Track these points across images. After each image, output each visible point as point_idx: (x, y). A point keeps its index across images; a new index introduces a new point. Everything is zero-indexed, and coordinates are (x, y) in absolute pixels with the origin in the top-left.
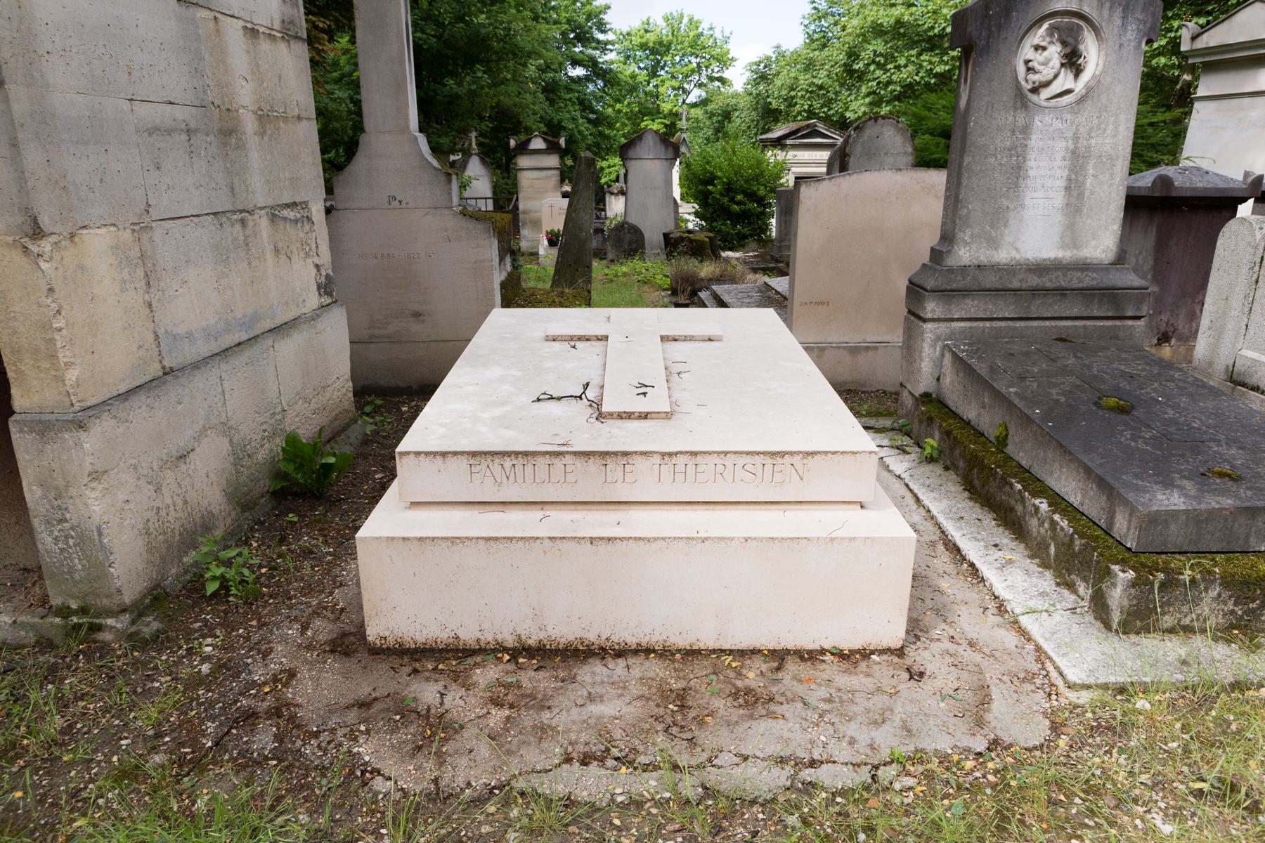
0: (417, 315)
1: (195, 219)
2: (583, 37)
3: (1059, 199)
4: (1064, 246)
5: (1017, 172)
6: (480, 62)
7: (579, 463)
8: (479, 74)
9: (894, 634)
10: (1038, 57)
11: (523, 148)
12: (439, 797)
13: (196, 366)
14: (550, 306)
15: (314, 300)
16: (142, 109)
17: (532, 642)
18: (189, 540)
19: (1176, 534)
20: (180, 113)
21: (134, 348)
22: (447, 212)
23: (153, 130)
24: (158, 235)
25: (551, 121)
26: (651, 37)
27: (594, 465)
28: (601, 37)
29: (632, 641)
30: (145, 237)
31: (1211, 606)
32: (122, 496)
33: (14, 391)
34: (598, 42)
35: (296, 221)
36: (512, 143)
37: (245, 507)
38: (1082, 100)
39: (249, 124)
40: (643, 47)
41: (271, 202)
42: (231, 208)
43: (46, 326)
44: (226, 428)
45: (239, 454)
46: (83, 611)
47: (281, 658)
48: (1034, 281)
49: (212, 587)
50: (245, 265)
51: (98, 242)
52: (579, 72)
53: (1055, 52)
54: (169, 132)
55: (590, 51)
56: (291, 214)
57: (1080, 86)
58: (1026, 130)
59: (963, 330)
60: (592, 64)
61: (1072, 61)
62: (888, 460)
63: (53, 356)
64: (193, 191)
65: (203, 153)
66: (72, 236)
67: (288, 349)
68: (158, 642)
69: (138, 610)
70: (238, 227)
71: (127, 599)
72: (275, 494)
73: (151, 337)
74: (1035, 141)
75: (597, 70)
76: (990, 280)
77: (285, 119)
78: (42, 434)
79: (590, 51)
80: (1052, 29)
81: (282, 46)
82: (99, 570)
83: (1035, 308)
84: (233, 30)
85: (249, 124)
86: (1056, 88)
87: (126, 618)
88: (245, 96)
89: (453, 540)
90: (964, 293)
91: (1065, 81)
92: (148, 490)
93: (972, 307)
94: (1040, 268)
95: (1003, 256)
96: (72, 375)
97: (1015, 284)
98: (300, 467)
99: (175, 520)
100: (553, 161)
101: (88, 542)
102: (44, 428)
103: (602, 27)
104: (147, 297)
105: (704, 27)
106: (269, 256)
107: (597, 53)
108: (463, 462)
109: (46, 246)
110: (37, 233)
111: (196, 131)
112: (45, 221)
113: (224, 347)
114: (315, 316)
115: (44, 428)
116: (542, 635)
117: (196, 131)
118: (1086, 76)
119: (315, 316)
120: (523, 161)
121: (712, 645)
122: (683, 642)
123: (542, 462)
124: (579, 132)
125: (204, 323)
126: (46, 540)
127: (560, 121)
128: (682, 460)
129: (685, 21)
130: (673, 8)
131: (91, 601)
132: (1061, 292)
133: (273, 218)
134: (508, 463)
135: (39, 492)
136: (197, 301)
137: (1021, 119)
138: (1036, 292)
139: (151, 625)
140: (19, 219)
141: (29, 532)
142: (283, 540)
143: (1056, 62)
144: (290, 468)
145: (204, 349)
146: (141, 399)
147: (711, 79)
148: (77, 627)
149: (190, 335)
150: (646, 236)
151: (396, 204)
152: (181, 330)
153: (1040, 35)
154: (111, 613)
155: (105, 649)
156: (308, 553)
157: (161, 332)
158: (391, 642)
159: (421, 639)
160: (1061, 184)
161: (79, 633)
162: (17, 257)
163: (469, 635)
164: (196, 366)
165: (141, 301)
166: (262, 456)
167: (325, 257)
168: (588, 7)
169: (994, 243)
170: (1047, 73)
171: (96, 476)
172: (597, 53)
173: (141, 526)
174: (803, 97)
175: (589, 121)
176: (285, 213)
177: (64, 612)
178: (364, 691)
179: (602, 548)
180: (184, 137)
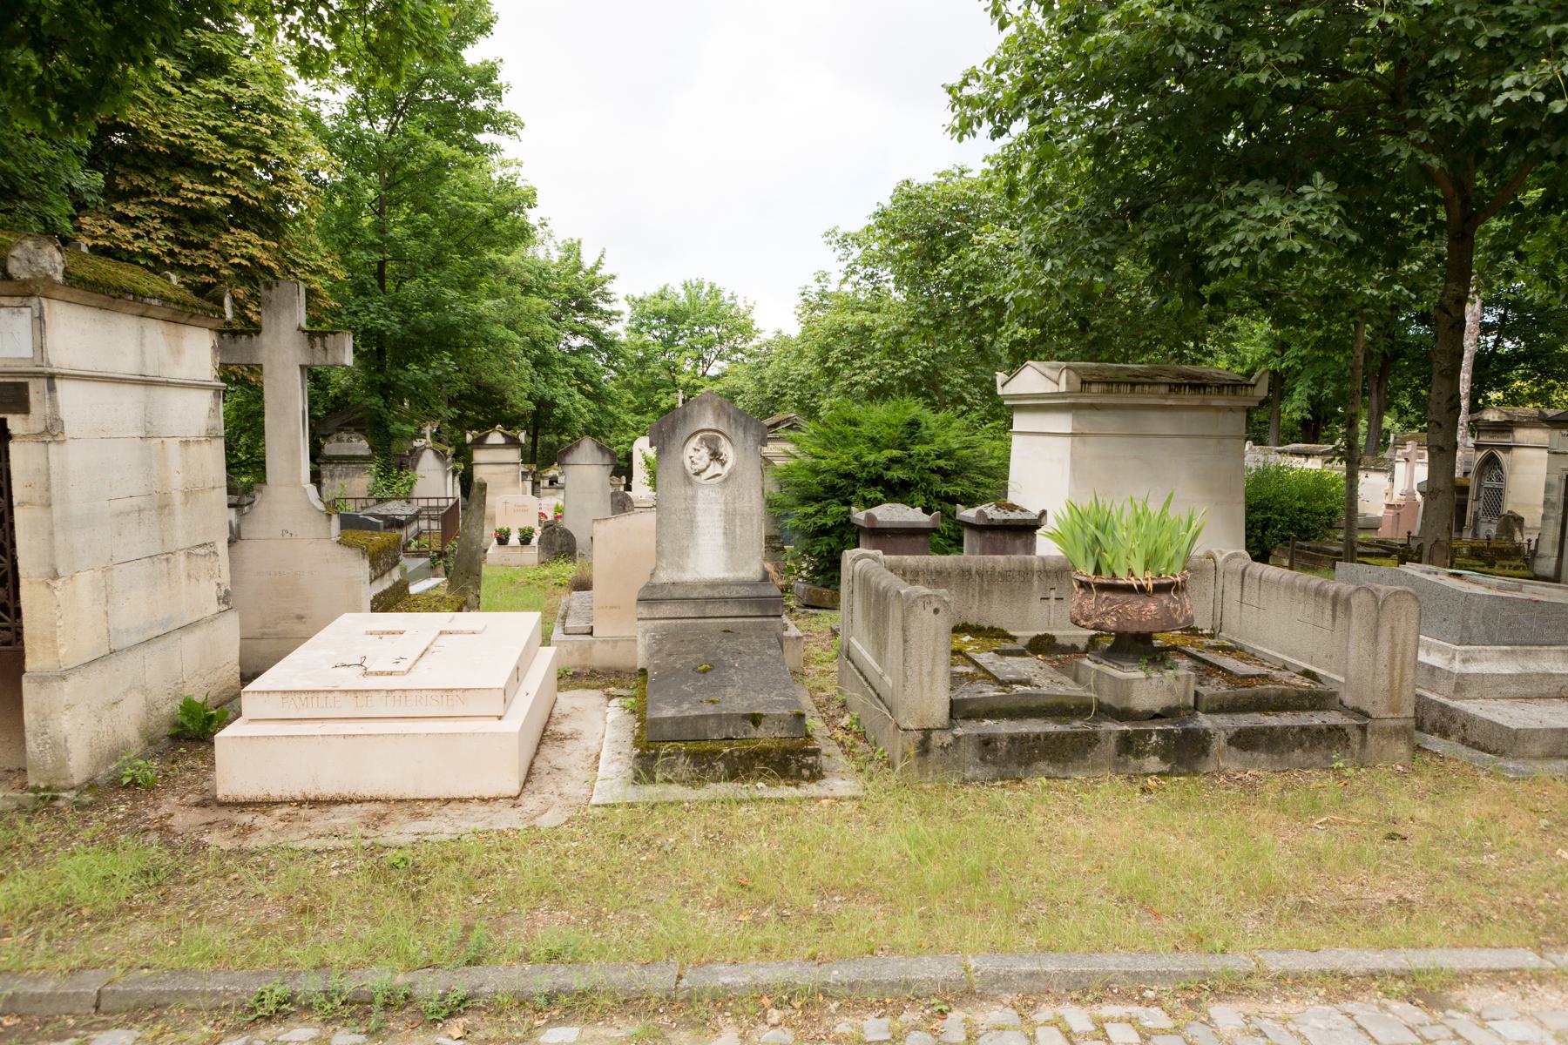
0: (300, 617)
2: (585, 307)
3: (720, 540)
4: (728, 570)
5: (691, 523)
6: (448, 347)
7: (343, 695)
8: (446, 361)
9: (513, 787)
10: (696, 455)
11: (480, 443)
13: (129, 649)
14: (426, 610)
15: (214, 607)
16: (115, 504)
17: (311, 797)
18: (114, 755)
19: (667, 730)
20: (135, 502)
23: (120, 514)
25: (542, 398)
26: (666, 306)
27: (350, 697)
28: (606, 307)
29: (368, 795)
31: (683, 767)
33: (27, 660)
34: (602, 312)
36: (469, 438)
37: (151, 743)
38: (726, 480)
39: (178, 498)
40: (658, 315)
43: (53, 625)
44: (144, 690)
45: (151, 707)
46: (48, 789)
47: (165, 809)
48: (708, 593)
49: (126, 780)
51: (84, 579)
52: (577, 343)
53: (705, 452)
54: (128, 514)
55: (593, 322)
56: (201, 551)
57: (724, 471)
58: (693, 498)
59: (662, 626)
60: (595, 335)
61: (716, 456)
63: (54, 641)
67: (190, 641)
68: (90, 806)
69: (80, 789)
71: (76, 781)
72: (171, 737)
74: (700, 505)
75: (603, 343)
76: (678, 593)
78: (41, 683)
79: (593, 322)
80: (702, 439)
81: (206, 445)
82: (62, 763)
83: (709, 611)
84: (173, 446)
85: (178, 498)
86: (709, 473)
87: (74, 793)
88: (177, 482)
89: (268, 737)
90: (661, 601)
91: (716, 468)
92: (94, 720)
93: (665, 610)
94: (713, 585)
95: (688, 577)
96: (62, 651)
97: (695, 595)
98: (192, 719)
99: (107, 742)
100: (513, 455)
101: (58, 746)
102: (42, 680)
103: (605, 297)
105: (726, 295)
107: (599, 323)
108: (279, 696)
109: (59, 583)
110: (56, 576)
112: (60, 571)
114: (213, 619)
115: (42, 680)
116: (317, 792)
118: (728, 466)
119: (213, 619)
120: (479, 456)
121: (413, 796)
122: (397, 795)
123: (322, 695)
124: (575, 409)
126: (32, 745)
127: (553, 398)
128: (397, 694)
129: (706, 289)
130: (692, 276)
131: (53, 782)
132: (725, 600)
133: (189, 555)
134: (303, 696)
135: (32, 717)
136: (136, 608)
137: (689, 491)
138: (708, 600)
139: (88, 798)
140: (47, 569)
141: (23, 741)
142: (174, 762)
143: (707, 458)
144: (185, 719)
145: (136, 639)
146: (96, 666)
147: (735, 350)
148: (43, 798)
149: (127, 631)
150: (578, 541)
153: (694, 442)
154: (65, 790)
155: (59, 810)
156: (191, 769)
158: (231, 799)
159: (248, 796)
160: (721, 531)
161: (46, 801)
162: (43, 588)
163: (276, 794)
164: (129, 649)
166: (166, 710)
167: (226, 578)
168: (591, 276)
169: (681, 568)
170: (701, 465)
171: (69, 707)
172: (599, 323)
174: (792, 388)
175: (588, 396)
177: (36, 790)
178: (211, 819)
179: (350, 740)
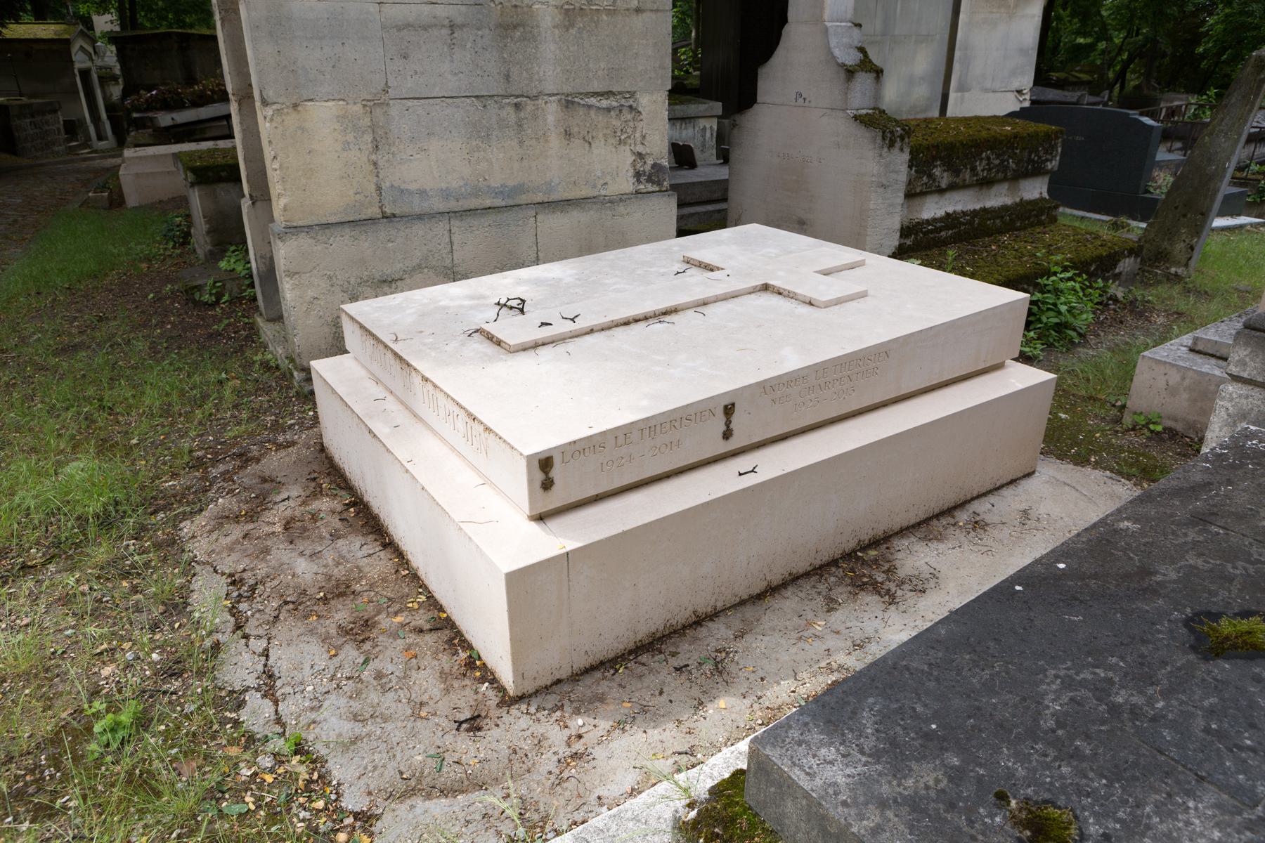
1: (450, 101)
12: (33, 116)
13: (420, 217)
21: (351, 193)
22: (841, 114)
24: (395, 109)
30: (378, 112)
32: (311, 293)
35: (609, 110)
41: (567, 89)
42: (502, 93)
50: (515, 143)
62: (697, 255)
64: (449, 77)
65: (469, 45)
66: (295, 106)
70: (511, 110)
73: (373, 187)
77: (611, 13)
104: (373, 157)
106: (555, 141)
111: (462, 26)
113: (466, 207)
117: (462, 26)
125: (444, 186)
151: (801, 100)
152: (413, 187)
157: (386, 185)
165: (365, 159)
173: (330, 319)
176: (593, 101)
180: (445, 32)
